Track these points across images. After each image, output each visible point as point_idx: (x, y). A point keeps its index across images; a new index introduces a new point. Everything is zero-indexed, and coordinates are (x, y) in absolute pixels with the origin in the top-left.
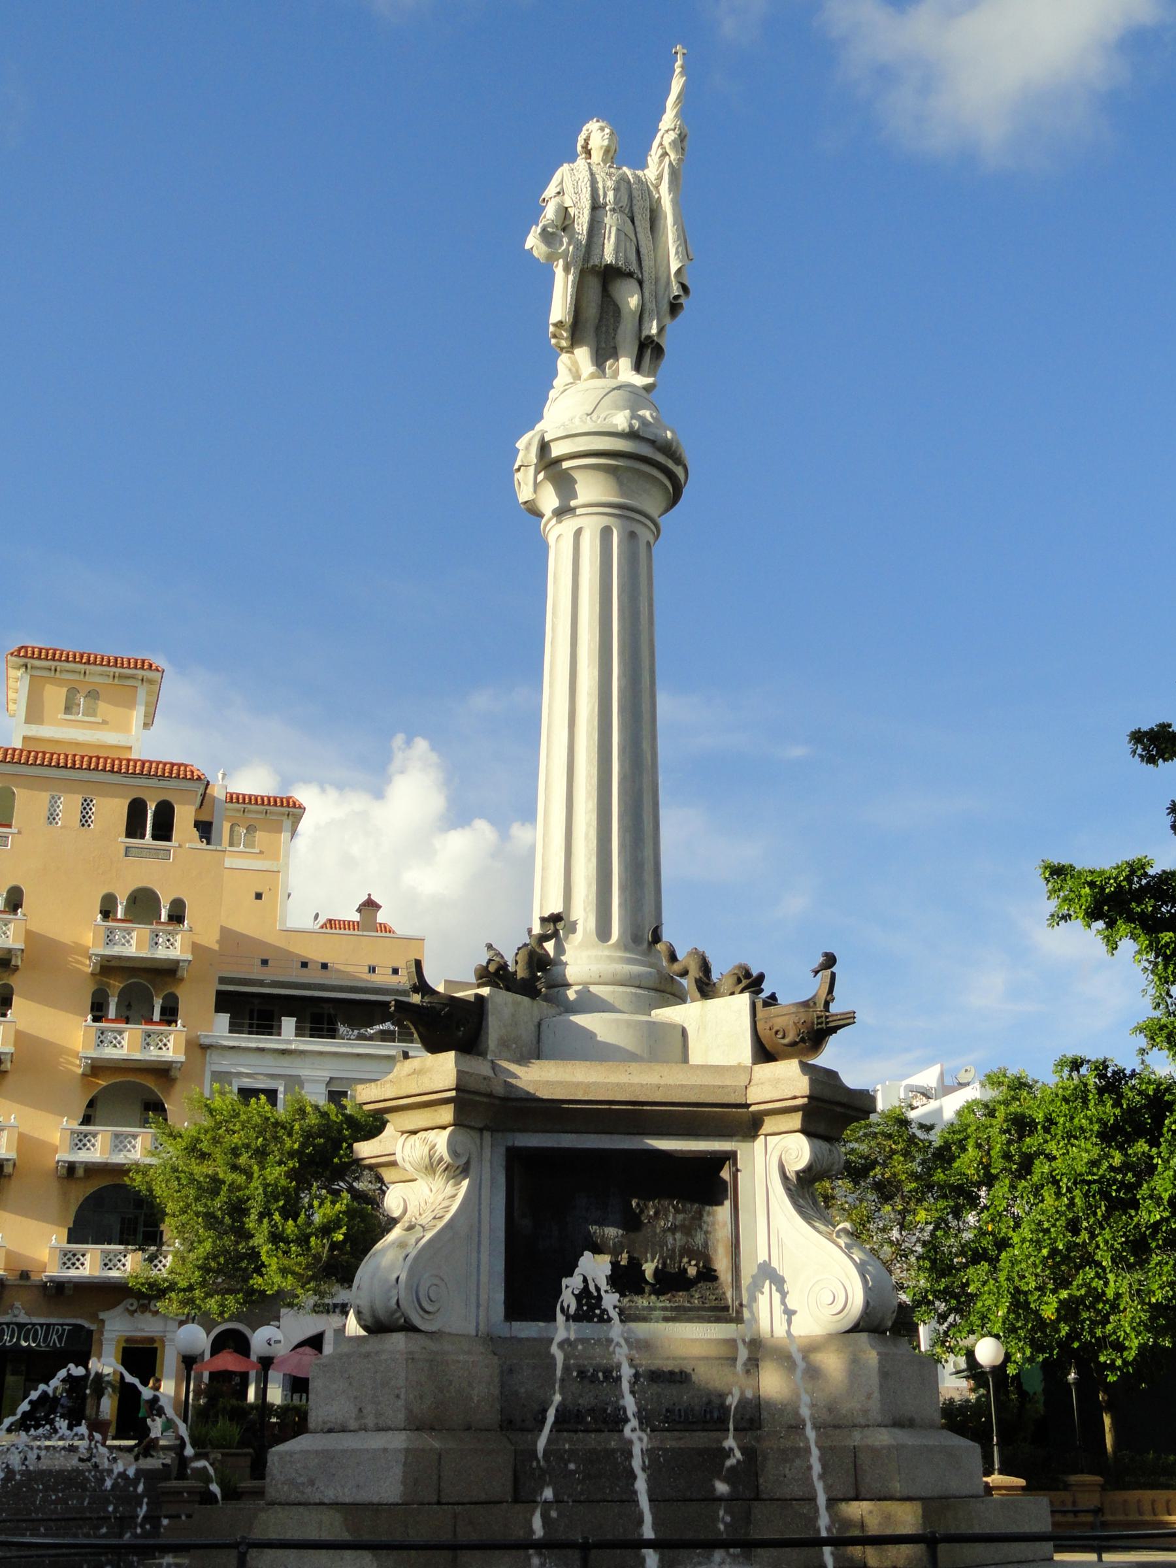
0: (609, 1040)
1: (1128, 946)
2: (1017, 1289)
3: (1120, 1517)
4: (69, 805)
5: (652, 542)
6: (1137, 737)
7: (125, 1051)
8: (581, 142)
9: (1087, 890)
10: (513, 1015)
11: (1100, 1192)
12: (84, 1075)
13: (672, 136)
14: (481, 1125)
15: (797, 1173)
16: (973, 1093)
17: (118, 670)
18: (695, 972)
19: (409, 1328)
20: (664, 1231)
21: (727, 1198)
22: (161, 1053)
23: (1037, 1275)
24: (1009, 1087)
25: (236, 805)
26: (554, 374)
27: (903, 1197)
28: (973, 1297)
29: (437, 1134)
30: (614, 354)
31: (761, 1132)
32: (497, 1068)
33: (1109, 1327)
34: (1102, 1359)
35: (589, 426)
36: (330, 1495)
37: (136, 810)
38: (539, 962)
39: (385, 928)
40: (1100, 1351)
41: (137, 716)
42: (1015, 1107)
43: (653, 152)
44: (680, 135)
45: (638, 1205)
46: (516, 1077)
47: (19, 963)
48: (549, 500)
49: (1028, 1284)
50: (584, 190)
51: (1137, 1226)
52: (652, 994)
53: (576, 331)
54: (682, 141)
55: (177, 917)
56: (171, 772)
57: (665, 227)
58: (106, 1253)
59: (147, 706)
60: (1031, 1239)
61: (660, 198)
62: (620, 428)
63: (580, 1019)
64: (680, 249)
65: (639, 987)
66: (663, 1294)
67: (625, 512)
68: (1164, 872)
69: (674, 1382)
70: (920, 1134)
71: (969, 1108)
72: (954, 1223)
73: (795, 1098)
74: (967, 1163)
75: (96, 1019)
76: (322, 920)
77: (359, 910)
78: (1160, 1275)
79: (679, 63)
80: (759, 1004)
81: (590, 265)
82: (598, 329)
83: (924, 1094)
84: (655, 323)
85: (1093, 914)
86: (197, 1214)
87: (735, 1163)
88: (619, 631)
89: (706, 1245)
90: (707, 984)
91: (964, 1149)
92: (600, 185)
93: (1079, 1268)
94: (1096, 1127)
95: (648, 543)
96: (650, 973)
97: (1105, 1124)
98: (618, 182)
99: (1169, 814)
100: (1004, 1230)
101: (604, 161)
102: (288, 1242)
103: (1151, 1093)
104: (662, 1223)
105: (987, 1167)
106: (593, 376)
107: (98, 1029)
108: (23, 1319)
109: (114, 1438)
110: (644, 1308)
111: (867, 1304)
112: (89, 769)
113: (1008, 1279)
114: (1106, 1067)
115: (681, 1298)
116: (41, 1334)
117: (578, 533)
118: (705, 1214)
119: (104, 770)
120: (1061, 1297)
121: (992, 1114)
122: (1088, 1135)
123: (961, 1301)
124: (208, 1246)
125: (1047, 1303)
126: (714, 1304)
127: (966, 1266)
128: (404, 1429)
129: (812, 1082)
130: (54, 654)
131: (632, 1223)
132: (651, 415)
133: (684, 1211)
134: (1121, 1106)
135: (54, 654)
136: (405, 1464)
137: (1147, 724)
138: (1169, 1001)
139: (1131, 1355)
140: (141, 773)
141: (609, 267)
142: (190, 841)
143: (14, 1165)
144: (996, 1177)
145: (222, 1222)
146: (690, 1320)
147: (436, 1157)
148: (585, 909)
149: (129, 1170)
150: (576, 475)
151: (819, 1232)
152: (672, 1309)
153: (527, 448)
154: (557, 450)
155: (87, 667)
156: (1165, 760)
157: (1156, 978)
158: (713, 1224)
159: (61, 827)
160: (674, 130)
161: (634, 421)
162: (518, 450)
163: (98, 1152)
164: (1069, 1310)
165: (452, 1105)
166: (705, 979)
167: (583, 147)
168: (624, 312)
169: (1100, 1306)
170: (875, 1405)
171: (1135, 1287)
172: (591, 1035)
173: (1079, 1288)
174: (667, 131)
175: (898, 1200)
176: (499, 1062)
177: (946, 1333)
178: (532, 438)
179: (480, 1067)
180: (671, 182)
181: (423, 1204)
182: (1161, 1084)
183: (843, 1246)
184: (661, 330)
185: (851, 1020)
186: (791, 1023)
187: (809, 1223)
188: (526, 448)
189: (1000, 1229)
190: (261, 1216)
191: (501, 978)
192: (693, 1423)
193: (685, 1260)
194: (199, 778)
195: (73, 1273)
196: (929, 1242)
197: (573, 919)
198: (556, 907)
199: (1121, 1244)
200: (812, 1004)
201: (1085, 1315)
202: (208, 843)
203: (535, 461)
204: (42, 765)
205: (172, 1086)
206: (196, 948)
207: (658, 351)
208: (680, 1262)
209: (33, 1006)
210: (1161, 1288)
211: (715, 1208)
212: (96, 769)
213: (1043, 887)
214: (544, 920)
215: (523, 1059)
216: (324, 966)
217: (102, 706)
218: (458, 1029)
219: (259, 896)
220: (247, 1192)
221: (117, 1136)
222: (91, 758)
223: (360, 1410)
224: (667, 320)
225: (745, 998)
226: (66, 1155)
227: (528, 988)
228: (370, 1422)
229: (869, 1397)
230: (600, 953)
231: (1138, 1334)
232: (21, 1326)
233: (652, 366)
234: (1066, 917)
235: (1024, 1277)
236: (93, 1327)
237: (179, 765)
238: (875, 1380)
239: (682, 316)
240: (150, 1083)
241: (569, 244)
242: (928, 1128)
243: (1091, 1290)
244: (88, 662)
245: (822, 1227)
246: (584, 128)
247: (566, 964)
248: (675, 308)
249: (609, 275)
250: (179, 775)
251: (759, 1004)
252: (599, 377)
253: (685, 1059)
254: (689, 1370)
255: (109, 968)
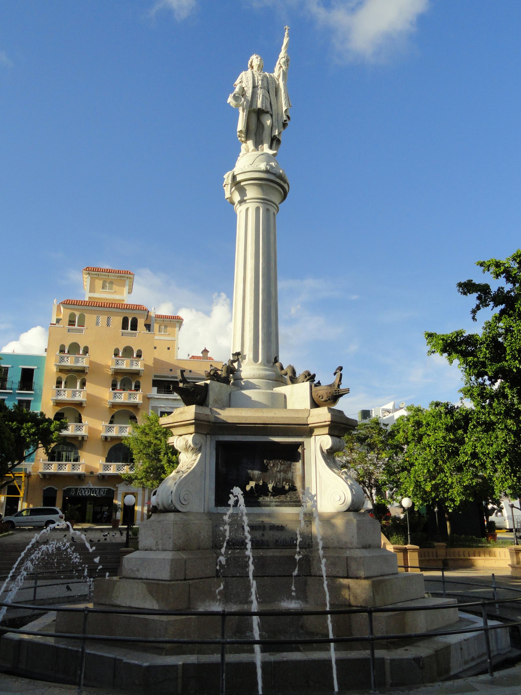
0: (256, 400)
1: (456, 362)
2: (417, 481)
3: (453, 557)
4: (103, 319)
5: (276, 212)
6: (460, 285)
7: (123, 400)
8: (249, 63)
9: (441, 341)
10: (219, 391)
11: (445, 450)
12: (110, 408)
13: (284, 60)
14: (206, 433)
15: (327, 450)
16: (404, 413)
17: (119, 275)
18: (290, 374)
19: (176, 511)
20: (277, 472)
21: (300, 459)
22: (134, 400)
23: (424, 476)
24: (414, 411)
25: (161, 319)
26: (240, 151)
27: (378, 448)
28: (402, 483)
29: (189, 436)
30: (262, 143)
31: (313, 435)
32: (212, 411)
33: (449, 494)
34: (446, 504)
35: (251, 169)
36: (144, 575)
37: (125, 321)
38: (231, 370)
39: (211, 358)
40: (446, 501)
41: (126, 289)
42: (416, 418)
43: (276, 66)
44: (286, 59)
45: (266, 462)
46: (219, 414)
47: (88, 371)
48: (237, 198)
49: (421, 479)
50: (250, 81)
51: (459, 461)
52: (274, 382)
53: (247, 133)
54: (287, 62)
55: (139, 356)
56: (136, 308)
57: (281, 94)
58: (118, 466)
59: (129, 286)
60: (422, 464)
61: (279, 83)
62: (262, 169)
63: (245, 392)
64: (286, 102)
65: (269, 379)
66: (276, 496)
67: (265, 201)
68: (469, 335)
69: (279, 530)
70: (383, 427)
71: (402, 418)
72: (395, 458)
73: (325, 422)
74: (400, 437)
75: (113, 389)
76: (190, 356)
77: (202, 353)
78: (467, 476)
79: (286, 32)
80: (313, 386)
81: (252, 109)
82: (256, 134)
83: (388, 412)
84: (277, 130)
85: (444, 351)
86: (144, 454)
87: (303, 446)
88: (262, 246)
89: (292, 477)
90: (294, 378)
91: (399, 432)
92: (256, 79)
93: (438, 473)
94: (444, 426)
95: (274, 213)
96: (273, 374)
97: (447, 425)
98: (263, 77)
99: (471, 313)
100: (412, 460)
101: (258, 70)
102: (173, 463)
103: (464, 414)
104: (276, 469)
105: (407, 439)
106: (253, 151)
107: (114, 393)
108: (92, 487)
109: (122, 525)
110: (269, 502)
111: (353, 500)
112: (109, 307)
113: (414, 477)
114: (448, 405)
115: (282, 497)
116: (98, 492)
117: (247, 209)
118: (292, 465)
119: (114, 307)
120: (432, 483)
121: (408, 420)
122: (441, 429)
123: (397, 484)
124: (147, 464)
125: (427, 486)
126: (295, 499)
127: (399, 472)
128: (172, 551)
129: (332, 415)
130: (98, 270)
131: (264, 469)
132: (275, 164)
133: (284, 464)
134: (453, 419)
135: (98, 270)
136: (171, 565)
137: (464, 280)
138: (471, 382)
139: (457, 503)
140: (126, 308)
141: (259, 109)
142: (143, 330)
143: (88, 437)
144: (410, 442)
145: (152, 457)
146: (286, 506)
147: (188, 445)
148: (249, 350)
149: (123, 439)
150: (246, 187)
151: (335, 473)
152: (279, 502)
153: (228, 178)
154: (239, 178)
155: (109, 274)
156: (470, 293)
157: (466, 374)
158: (295, 469)
159: (101, 327)
160: (284, 57)
161: (267, 166)
162: (224, 179)
163: (114, 433)
164: (435, 488)
165: (194, 426)
166: (293, 376)
167: (250, 65)
168: (265, 126)
169: (446, 486)
170: (355, 541)
171: (458, 480)
172: (250, 398)
173: (439, 480)
174: (282, 58)
175: (376, 449)
176: (213, 409)
177: (393, 494)
178: (229, 174)
179: (205, 411)
180: (283, 77)
181: (184, 463)
182: (468, 411)
183: (344, 478)
184: (279, 133)
185: (348, 392)
186: (325, 393)
187: (331, 469)
188: (228, 177)
189: (411, 460)
190: (165, 454)
191: (215, 377)
192: (286, 545)
193: (284, 483)
194: (146, 310)
195: (107, 472)
196: (387, 464)
197: (244, 354)
198: (238, 350)
199: (453, 468)
200: (333, 386)
201: (441, 490)
202: (149, 331)
203: (231, 182)
204: (94, 306)
205: (138, 411)
206: (145, 366)
207: (279, 141)
208: (283, 484)
209: (93, 385)
210: (467, 480)
211: (296, 463)
212: (112, 307)
213: (426, 341)
214: (233, 355)
215: (223, 408)
216: (190, 371)
217: (115, 287)
218: (197, 396)
219: (169, 349)
220: (160, 446)
221: (121, 427)
222: (110, 303)
223: (157, 542)
224: (282, 130)
225: (307, 384)
226: (104, 434)
227: (226, 381)
228: (160, 547)
229: (353, 537)
230: (254, 367)
231: (460, 496)
232: (91, 489)
233: (276, 147)
234: (433, 352)
235: (419, 476)
236: (114, 489)
237: (139, 306)
238: (355, 531)
239: (288, 128)
240: (131, 410)
241: (244, 101)
242: (386, 425)
243: (443, 480)
244: (109, 272)
245: (336, 471)
246: (251, 58)
247: (242, 371)
248: (285, 125)
249: (260, 113)
250: (139, 308)
251: (313, 386)
252: (256, 151)
253: (285, 407)
254: (284, 525)
255: (117, 373)
